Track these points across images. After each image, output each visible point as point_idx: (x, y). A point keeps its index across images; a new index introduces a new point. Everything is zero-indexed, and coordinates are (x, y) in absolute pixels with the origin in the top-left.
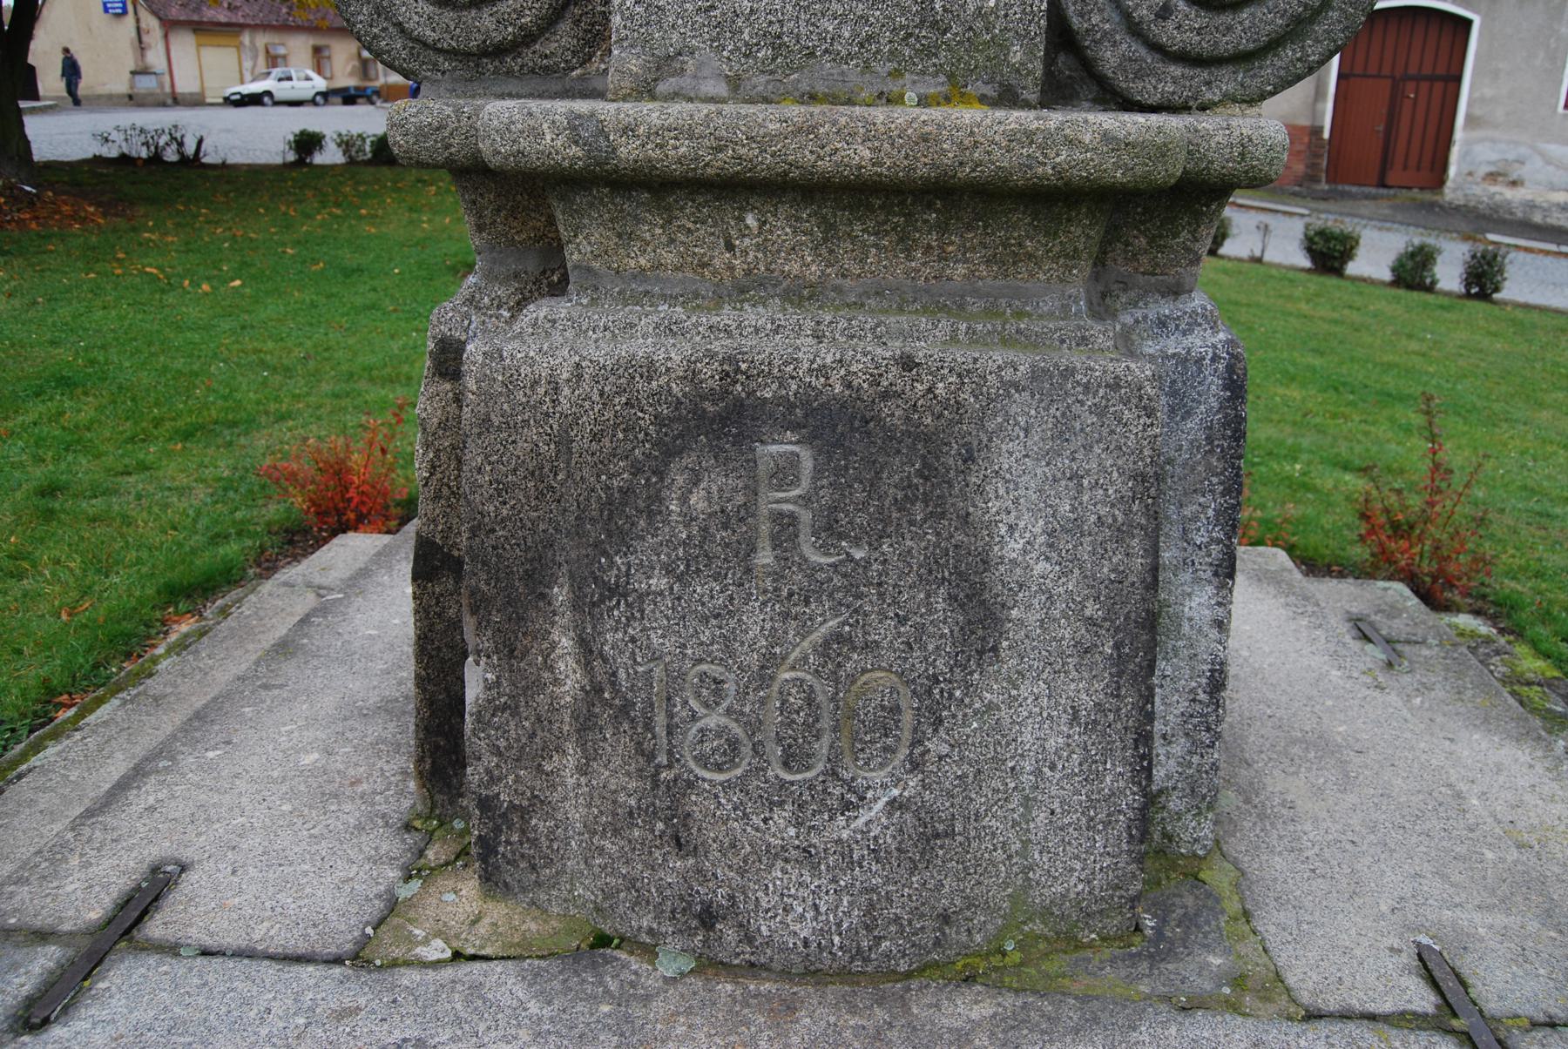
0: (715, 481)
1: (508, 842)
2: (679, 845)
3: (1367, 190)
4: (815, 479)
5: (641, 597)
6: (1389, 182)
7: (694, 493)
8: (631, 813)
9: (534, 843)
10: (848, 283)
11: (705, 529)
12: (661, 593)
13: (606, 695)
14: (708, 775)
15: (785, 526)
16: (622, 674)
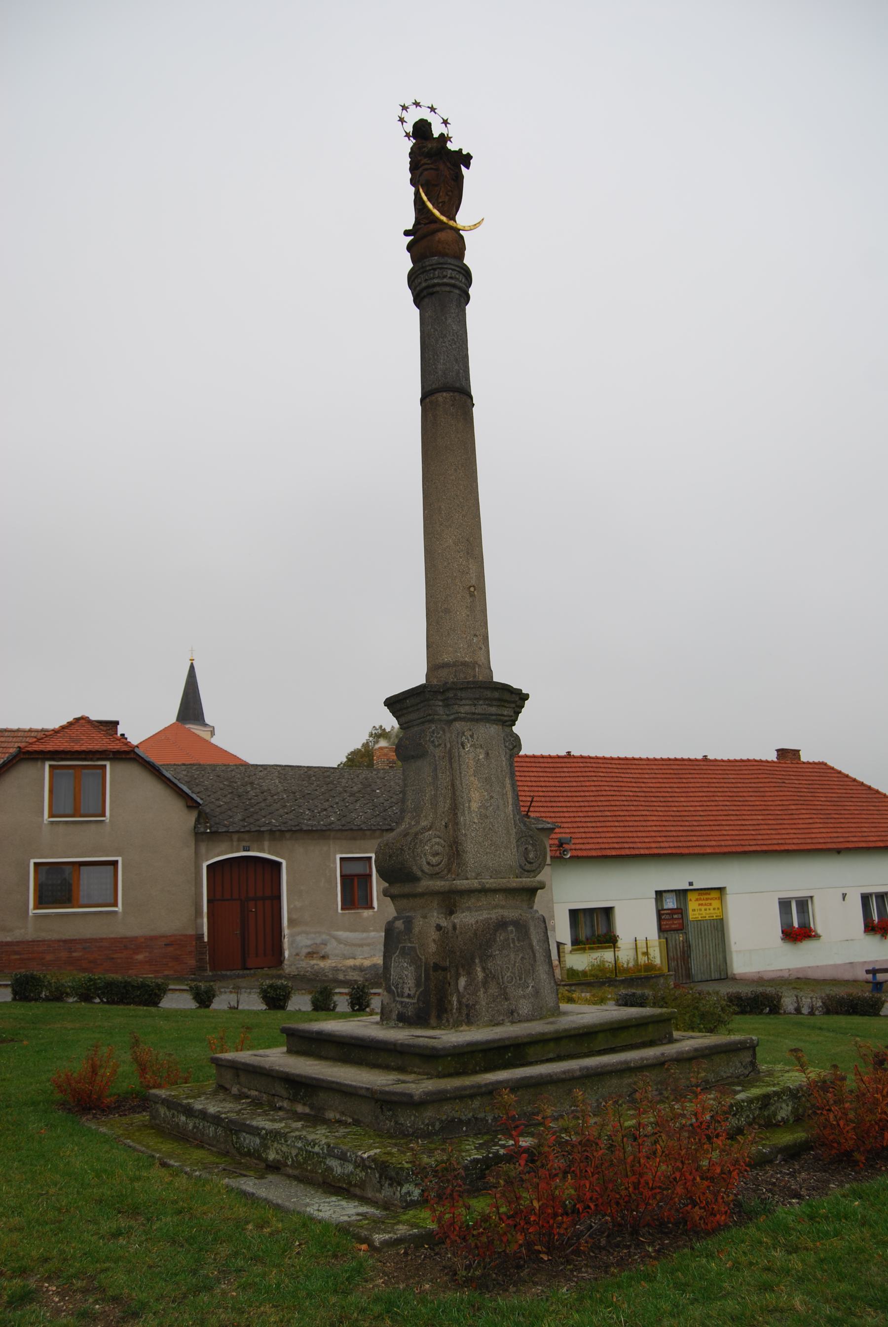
0: (503, 934)
7: (501, 937)
15: (513, 939)
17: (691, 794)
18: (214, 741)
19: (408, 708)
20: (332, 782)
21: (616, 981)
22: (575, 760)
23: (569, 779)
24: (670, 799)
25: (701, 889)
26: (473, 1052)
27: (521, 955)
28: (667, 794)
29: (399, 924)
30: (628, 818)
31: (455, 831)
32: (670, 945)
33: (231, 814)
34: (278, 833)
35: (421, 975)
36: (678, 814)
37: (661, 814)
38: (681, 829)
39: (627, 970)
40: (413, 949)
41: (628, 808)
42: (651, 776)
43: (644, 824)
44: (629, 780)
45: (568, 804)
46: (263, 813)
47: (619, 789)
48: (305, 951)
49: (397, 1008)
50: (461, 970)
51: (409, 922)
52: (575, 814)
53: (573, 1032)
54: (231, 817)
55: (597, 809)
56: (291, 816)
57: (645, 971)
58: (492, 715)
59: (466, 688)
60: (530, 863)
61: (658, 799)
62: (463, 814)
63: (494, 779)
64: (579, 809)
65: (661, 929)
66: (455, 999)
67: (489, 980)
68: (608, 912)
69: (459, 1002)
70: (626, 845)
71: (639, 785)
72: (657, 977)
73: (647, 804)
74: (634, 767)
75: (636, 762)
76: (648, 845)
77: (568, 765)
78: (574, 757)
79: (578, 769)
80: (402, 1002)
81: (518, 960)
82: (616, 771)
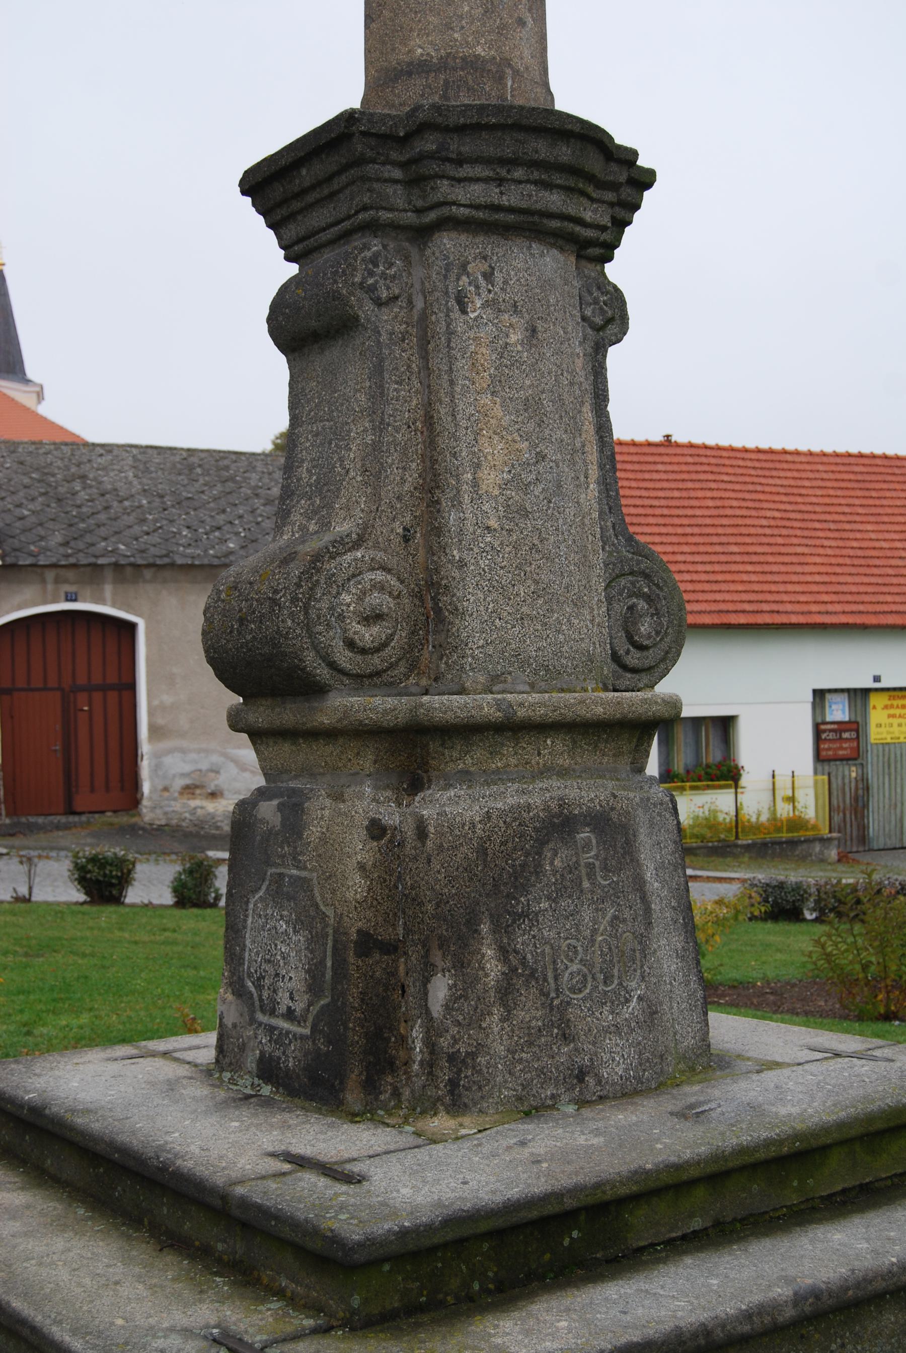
0: (563, 853)
1: (466, 1077)
2: (565, 1038)
3: (56, 819)
4: (598, 847)
5: (536, 914)
6: (78, 806)
7: (556, 860)
8: (540, 1030)
9: (480, 1072)
10: (577, 767)
11: (562, 875)
12: (546, 910)
13: (520, 971)
14: (575, 996)
16: (529, 956)
17: (886, 519)
18: (44, 410)
19: (304, 192)
20: (232, 479)
21: (736, 846)
22: (679, 451)
23: (665, 485)
24: (847, 526)
25: (895, 689)
26: (461, 1242)
27: (611, 912)
28: (842, 518)
29: (268, 810)
30: (770, 559)
31: (431, 551)
32: (834, 786)
33: (43, 533)
34: (129, 570)
35: (322, 962)
36: (860, 553)
37: (829, 552)
38: (866, 580)
39: (756, 828)
40: (304, 884)
41: (772, 540)
42: (815, 483)
43: (799, 569)
44: (774, 489)
45: (663, 530)
46: (103, 531)
47: (757, 505)
48: (179, 783)
49: (258, 1044)
50: (437, 957)
51: (294, 810)
52: (676, 549)
53: (761, 1155)
54: (42, 538)
55: (715, 539)
56: (155, 538)
57: (789, 830)
58: (551, 216)
59: (478, 127)
60: (641, 648)
61: (825, 526)
62: (456, 502)
63: (548, 406)
64: (683, 540)
65: (819, 758)
66: (417, 1034)
67: (519, 983)
68: (725, 725)
69: (431, 1045)
70: (765, 607)
71: (792, 499)
72: (808, 841)
73: (806, 533)
74: (785, 466)
75: (789, 458)
76: (805, 608)
77: (666, 459)
78: (677, 445)
79: (684, 468)
80: (271, 1029)
81: (604, 924)
82: (753, 472)
